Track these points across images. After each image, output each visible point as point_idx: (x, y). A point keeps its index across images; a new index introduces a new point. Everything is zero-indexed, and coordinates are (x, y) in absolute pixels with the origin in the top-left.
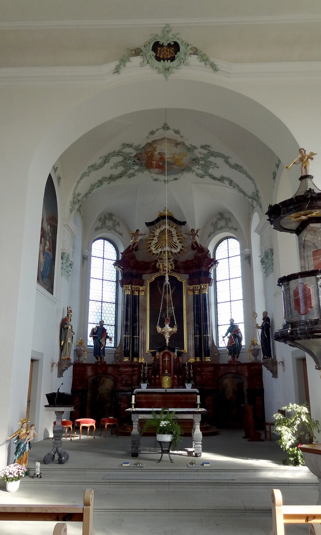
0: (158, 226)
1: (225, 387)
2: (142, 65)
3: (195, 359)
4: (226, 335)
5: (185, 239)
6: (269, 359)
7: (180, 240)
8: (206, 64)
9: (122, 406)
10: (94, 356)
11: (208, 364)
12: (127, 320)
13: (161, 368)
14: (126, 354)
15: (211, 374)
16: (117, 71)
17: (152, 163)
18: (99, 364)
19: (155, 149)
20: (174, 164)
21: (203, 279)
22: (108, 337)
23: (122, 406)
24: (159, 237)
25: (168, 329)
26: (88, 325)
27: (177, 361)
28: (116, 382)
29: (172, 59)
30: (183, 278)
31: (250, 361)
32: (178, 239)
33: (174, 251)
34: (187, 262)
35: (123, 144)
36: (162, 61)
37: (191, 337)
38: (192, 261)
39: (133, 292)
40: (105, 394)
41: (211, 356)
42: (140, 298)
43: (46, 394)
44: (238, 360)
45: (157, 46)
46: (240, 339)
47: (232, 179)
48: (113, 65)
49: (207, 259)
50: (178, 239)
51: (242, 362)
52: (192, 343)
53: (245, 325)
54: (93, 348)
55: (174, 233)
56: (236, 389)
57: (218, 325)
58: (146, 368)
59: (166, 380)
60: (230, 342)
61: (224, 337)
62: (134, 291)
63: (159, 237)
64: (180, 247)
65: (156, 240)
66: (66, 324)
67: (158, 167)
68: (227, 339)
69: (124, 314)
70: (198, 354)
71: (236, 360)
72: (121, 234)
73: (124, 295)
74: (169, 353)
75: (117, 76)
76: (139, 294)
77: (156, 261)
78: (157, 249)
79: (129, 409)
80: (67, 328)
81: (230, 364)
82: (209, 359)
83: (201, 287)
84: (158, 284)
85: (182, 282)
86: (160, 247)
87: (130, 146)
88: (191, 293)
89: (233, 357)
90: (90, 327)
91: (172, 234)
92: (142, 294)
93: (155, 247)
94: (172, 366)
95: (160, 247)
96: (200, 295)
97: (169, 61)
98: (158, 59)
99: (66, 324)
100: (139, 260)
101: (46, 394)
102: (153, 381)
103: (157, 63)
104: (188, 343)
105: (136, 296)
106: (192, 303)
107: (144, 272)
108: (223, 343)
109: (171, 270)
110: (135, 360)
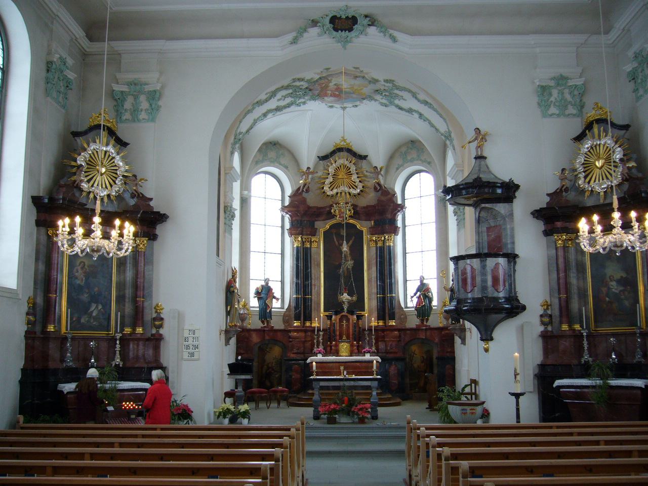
0: (333, 162)
1: (413, 354)
2: (319, 35)
3: (378, 323)
4: (415, 294)
5: (365, 176)
6: (458, 325)
7: (360, 179)
8: (385, 35)
9: (293, 377)
10: (260, 319)
11: (392, 329)
12: (297, 277)
13: (338, 333)
14: (297, 318)
15: (395, 339)
16: (294, 41)
17: (326, 93)
18: (266, 329)
19: (330, 81)
20: (354, 93)
21: (387, 228)
22: (274, 297)
23: (293, 377)
24: (334, 175)
25: (345, 297)
26: (249, 282)
27: (356, 325)
28: (285, 348)
29: (350, 30)
30: (363, 226)
31: (441, 325)
32: (358, 177)
33: (353, 191)
34: (367, 207)
35: (293, 79)
36: (340, 31)
37: (374, 296)
38: (374, 206)
39: (303, 243)
40: (272, 363)
41: (396, 318)
42: (313, 250)
43: (228, 364)
44: (428, 324)
45: (333, 20)
46: (430, 300)
47: (423, 113)
48: (290, 37)
49: (392, 205)
50: (358, 177)
51: (432, 326)
52: (374, 303)
53: (438, 280)
54: (258, 309)
55: (353, 169)
56: (425, 357)
57: (407, 281)
58: (321, 333)
59: (344, 347)
60: (419, 303)
61: (412, 297)
62: (305, 241)
63: (334, 175)
64: (360, 186)
65: (330, 179)
66: (232, 287)
67: (333, 95)
68: (415, 300)
69: (293, 270)
70: (381, 316)
71: (425, 323)
72: (286, 167)
73: (293, 247)
74: (347, 316)
75: (294, 47)
76: (311, 245)
77: (331, 206)
78: (332, 190)
79: (312, 377)
80: (234, 291)
81: (417, 330)
82: (395, 322)
83: (385, 237)
84: (334, 234)
85: (363, 231)
86: (336, 187)
87: (302, 80)
88: (373, 244)
89: (422, 321)
90: (254, 286)
91: (350, 172)
92: (314, 245)
93: (331, 186)
94: (351, 331)
95: (336, 187)
96: (384, 247)
97: (347, 31)
98: (336, 30)
99: (232, 287)
100: (311, 205)
101: (228, 364)
102: (329, 349)
103: (335, 33)
104: (370, 302)
105: (308, 247)
106: (375, 256)
107: (316, 219)
108: (412, 303)
109: (350, 216)
110: (308, 324)
